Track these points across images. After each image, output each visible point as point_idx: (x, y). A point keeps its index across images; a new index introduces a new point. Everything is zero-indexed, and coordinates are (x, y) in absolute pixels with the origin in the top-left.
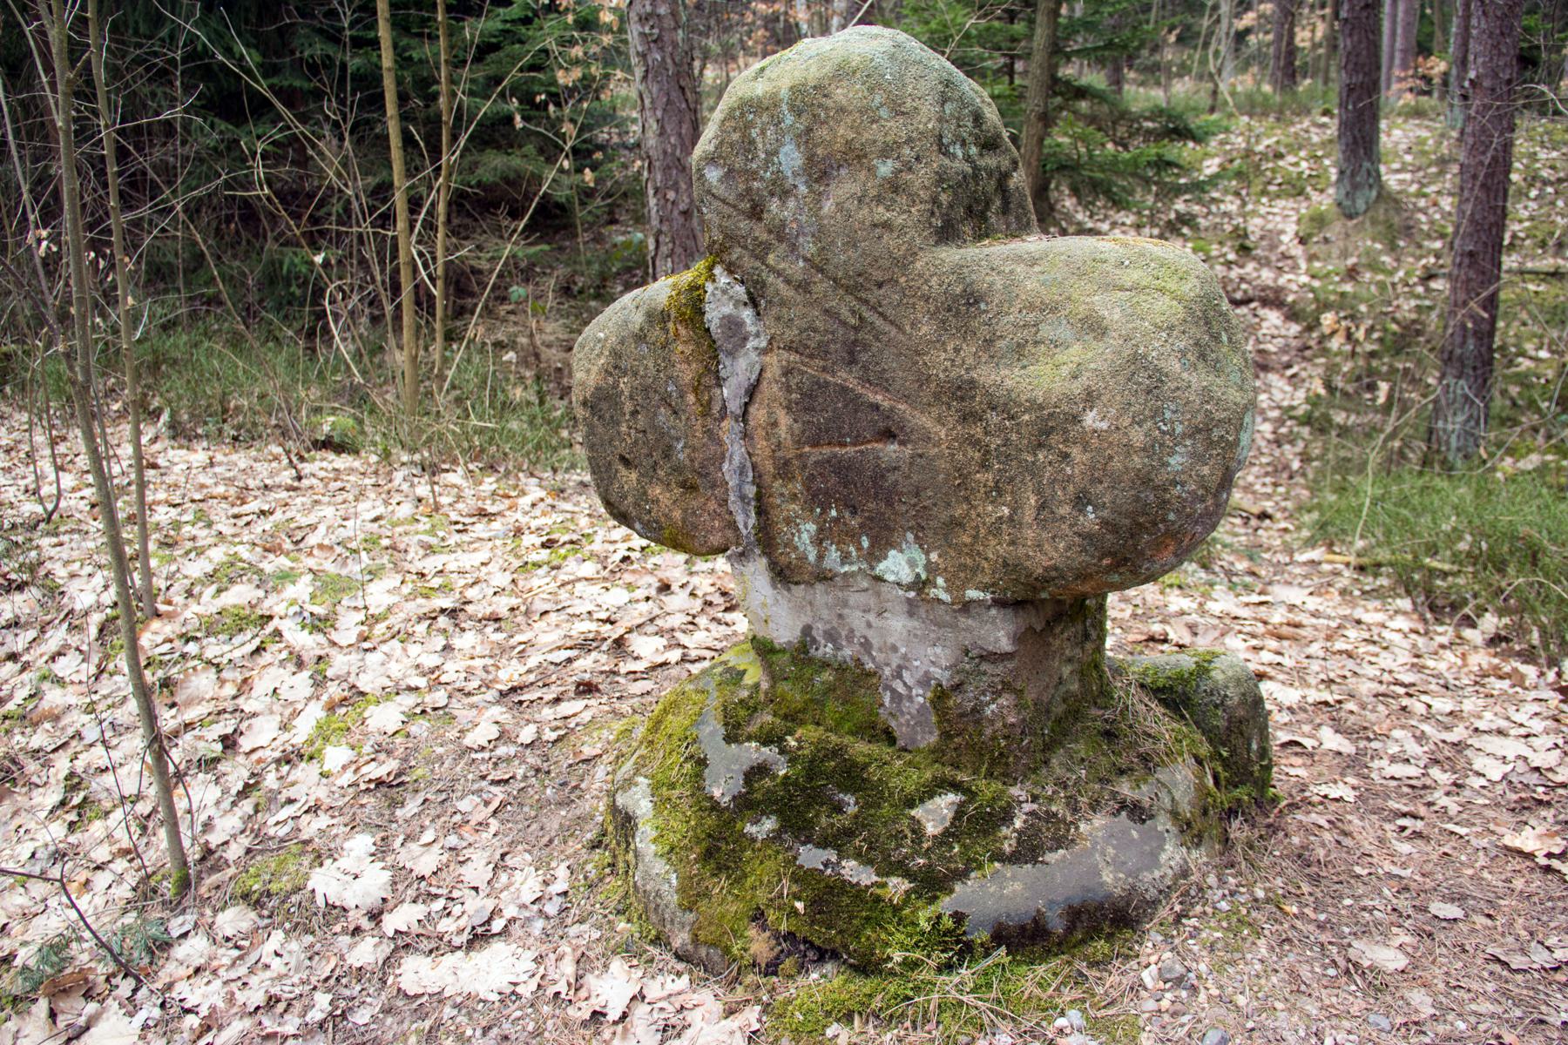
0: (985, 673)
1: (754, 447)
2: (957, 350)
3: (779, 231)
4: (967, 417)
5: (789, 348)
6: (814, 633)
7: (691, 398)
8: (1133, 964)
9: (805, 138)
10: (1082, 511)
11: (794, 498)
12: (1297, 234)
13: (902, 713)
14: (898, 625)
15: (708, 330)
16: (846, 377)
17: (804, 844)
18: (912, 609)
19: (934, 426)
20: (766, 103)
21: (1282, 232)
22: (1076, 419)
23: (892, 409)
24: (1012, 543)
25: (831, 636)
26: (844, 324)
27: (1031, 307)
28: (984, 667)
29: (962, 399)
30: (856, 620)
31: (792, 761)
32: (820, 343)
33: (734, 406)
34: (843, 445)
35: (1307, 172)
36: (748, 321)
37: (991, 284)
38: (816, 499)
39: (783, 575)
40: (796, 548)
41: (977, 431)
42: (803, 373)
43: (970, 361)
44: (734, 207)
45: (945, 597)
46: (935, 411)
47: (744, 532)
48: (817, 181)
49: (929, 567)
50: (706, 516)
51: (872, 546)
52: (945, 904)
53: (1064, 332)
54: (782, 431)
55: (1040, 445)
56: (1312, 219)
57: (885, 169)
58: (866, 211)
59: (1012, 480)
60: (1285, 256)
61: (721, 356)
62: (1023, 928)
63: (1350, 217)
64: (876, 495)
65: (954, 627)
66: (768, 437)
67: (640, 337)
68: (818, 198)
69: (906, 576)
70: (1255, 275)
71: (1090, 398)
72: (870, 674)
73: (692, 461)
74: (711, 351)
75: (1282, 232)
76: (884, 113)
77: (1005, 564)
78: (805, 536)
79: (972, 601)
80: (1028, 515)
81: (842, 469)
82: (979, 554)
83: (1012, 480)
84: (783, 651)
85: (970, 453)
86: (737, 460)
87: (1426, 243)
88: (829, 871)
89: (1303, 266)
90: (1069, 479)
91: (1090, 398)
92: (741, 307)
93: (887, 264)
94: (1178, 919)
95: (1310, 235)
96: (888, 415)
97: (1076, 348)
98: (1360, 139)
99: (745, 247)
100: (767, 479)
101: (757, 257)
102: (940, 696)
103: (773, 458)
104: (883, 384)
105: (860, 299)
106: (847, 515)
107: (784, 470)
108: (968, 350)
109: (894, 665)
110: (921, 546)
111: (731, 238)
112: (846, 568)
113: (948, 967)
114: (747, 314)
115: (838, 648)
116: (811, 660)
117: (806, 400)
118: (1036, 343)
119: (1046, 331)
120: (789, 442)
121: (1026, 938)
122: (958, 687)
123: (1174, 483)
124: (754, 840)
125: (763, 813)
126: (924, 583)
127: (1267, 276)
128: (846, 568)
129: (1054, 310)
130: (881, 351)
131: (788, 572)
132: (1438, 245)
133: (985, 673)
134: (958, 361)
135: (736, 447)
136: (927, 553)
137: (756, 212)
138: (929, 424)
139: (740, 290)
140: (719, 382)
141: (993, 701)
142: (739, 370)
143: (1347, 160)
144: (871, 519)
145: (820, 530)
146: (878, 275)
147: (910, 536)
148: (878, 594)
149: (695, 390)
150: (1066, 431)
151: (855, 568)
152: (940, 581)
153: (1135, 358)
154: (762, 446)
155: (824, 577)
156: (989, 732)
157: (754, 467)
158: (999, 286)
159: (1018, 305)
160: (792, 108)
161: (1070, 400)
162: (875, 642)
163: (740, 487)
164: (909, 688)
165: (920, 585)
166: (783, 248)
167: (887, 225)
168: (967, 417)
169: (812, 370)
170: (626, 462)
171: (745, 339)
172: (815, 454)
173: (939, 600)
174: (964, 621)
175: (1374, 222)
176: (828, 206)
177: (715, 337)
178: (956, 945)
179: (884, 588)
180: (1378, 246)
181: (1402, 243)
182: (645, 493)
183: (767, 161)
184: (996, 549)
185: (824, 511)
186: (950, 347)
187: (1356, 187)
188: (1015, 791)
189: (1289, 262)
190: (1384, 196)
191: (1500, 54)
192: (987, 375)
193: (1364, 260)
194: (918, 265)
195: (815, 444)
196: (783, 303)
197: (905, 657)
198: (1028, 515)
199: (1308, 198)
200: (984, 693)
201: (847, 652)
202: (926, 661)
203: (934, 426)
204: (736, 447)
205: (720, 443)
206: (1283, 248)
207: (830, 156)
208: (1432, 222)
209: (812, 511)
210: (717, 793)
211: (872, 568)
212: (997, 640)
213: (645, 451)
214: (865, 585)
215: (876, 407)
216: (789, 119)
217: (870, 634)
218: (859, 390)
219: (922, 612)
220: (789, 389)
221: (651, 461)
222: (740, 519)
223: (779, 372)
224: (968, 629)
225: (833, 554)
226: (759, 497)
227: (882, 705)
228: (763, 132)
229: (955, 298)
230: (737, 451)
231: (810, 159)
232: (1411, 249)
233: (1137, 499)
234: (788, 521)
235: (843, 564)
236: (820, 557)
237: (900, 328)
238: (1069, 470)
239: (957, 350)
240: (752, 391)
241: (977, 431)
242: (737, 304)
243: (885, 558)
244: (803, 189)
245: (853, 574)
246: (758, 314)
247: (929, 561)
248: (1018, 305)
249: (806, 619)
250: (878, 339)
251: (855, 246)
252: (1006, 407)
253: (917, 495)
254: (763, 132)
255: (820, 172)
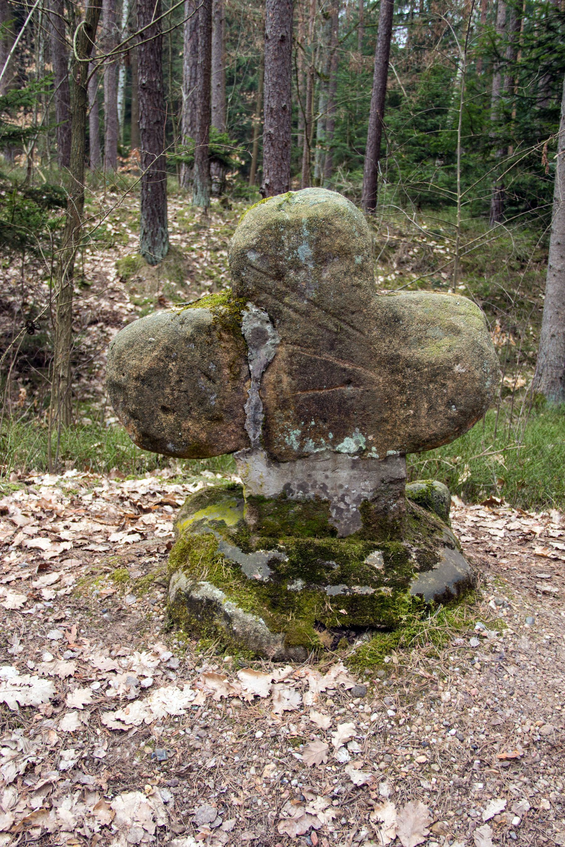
0: (391, 490)
1: (265, 394)
2: (390, 342)
3: (294, 287)
4: (393, 372)
5: (294, 343)
6: (292, 487)
7: (226, 371)
8: (483, 602)
9: (316, 243)
10: (450, 408)
11: (288, 418)
12: (117, 274)
13: (342, 519)
14: (344, 474)
15: (243, 335)
16: (330, 357)
17: (325, 586)
18: (354, 465)
19: (378, 378)
20: (293, 224)
21: (107, 274)
22: (450, 369)
23: (354, 370)
24: (414, 426)
25: (302, 487)
26: (330, 331)
27: (422, 322)
28: (391, 487)
29: (393, 363)
30: (319, 476)
31: (289, 554)
32: (314, 341)
33: (256, 374)
34: (320, 389)
35: (113, 232)
36: (269, 331)
37: (404, 313)
38: (302, 417)
39: (275, 459)
40: (286, 444)
41: (399, 377)
42: (301, 355)
43: (396, 346)
44: (265, 273)
45: (375, 456)
46: (377, 370)
47: (253, 439)
48: (320, 263)
49: (367, 443)
50: (225, 434)
51: (335, 437)
52: (411, 592)
53: (438, 333)
54: (285, 385)
55: (431, 382)
56: (128, 265)
57: (359, 260)
58: (348, 279)
59: (416, 397)
60: (113, 290)
61: (250, 349)
62: (444, 595)
63: (152, 264)
64: (340, 411)
65: (376, 470)
66: (275, 388)
67: (190, 340)
68: (320, 271)
69: (353, 448)
70: (96, 303)
71: (458, 360)
72: (326, 502)
73: (221, 405)
74: (243, 347)
75: (107, 274)
76: (356, 234)
77: (410, 436)
78: (293, 437)
79: (390, 456)
80: (423, 412)
81: (321, 402)
82: (395, 433)
83: (416, 397)
84: (270, 500)
85: (394, 387)
86: (254, 401)
87: (202, 282)
88: (348, 593)
89: (128, 297)
90: (445, 395)
91: (458, 360)
92: (265, 324)
93: (358, 303)
94: (485, 583)
95: (128, 276)
96: (351, 373)
97: (446, 340)
98: (155, 212)
99: (270, 294)
100: (271, 410)
101: (276, 299)
102: (365, 507)
103: (277, 399)
104: (350, 358)
105: (340, 320)
106: (321, 423)
107: (283, 405)
108: (396, 342)
109: (340, 495)
110: (363, 434)
111: (262, 289)
112: (318, 450)
113: (423, 618)
114: (268, 327)
115: (306, 492)
116: (289, 502)
117: (301, 369)
118: (426, 338)
119: (430, 333)
120: (288, 390)
121: (446, 598)
122: (375, 500)
123: (487, 393)
124: (296, 592)
125: (293, 579)
126: (364, 451)
127: (105, 304)
128: (318, 450)
129: (433, 323)
130: (350, 344)
131: (279, 457)
132: (209, 283)
133: (391, 490)
134: (391, 347)
135: (254, 395)
136: (366, 437)
137: (280, 276)
138: (374, 376)
139: (265, 315)
140: (247, 361)
141: (394, 502)
142: (259, 357)
143: (149, 225)
144: (336, 424)
145: (303, 433)
146: (352, 308)
147: (357, 430)
148: (335, 461)
149: (230, 367)
150: (444, 374)
151: (323, 449)
152: (374, 449)
153: (474, 343)
154: (270, 393)
155: (302, 456)
156: (391, 518)
157: (264, 404)
158: (406, 313)
159: (416, 321)
160: (309, 227)
161: (449, 361)
162: (329, 486)
163: (254, 416)
164: (348, 505)
165: (361, 452)
166: (293, 295)
167: (359, 286)
168: (393, 372)
169: (308, 353)
170: (165, 409)
171: (267, 339)
172: (303, 395)
173: (372, 458)
174: (383, 466)
175: (169, 268)
176: (325, 276)
177: (247, 338)
178: (421, 607)
179: (339, 457)
180: (173, 284)
181: (188, 283)
182: (180, 426)
183: (289, 252)
184: (404, 430)
185: (306, 422)
186: (387, 341)
187: (154, 243)
188: (405, 544)
189: (117, 294)
190: (172, 251)
191: (282, 171)
192: (405, 352)
193: (167, 293)
194: (372, 304)
195: (304, 390)
196: (292, 321)
197: (347, 490)
198: (423, 412)
199: (117, 250)
200: (390, 500)
201: (312, 493)
202: (359, 489)
203: (378, 378)
204: (254, 395)
205: (243, 393)
206: (110, 285)
207: (330, 252)
208: (203, 268)
209: (298, 423)
210: (259, 577)
211: (334, 448)
212: (400, 472)
213: (185, 402)
214: (329, 457)
215: (345, 370)
216: (306, 233)
217: (327, 482)
218: (336, 362)
219: (361, 465)
220: (292, 364)
221: (188, 408)
222: (251, 433)
223: (286, 355)
224: (385, 470)
225: (311, 443)
226: (265, 420)
227: (331, 517)
228: (289, 238)
229: (389, 319)
230: (254, 397)
231: (318, 253)
232: (194, 286)
233: (475, 400)
234: (282, 431)
235: (316, 447)
236: (301, 447)
237: (362, 333)
238: (445, 391)
239: (390, 342)
240: (268, 366)
241: (399, 377)
242: (263, 321)
243: (343, 441)
244: (311, 267)
245: (322, 453)
246: (274, 327)
247: (367, 440)
248: (416, 321)
249: (286, 481)
250: (349, 338)
251: (341, 295)
252: (416, 366)
253: (364, 409)
254: (289, 238)
255: (321, 259)
